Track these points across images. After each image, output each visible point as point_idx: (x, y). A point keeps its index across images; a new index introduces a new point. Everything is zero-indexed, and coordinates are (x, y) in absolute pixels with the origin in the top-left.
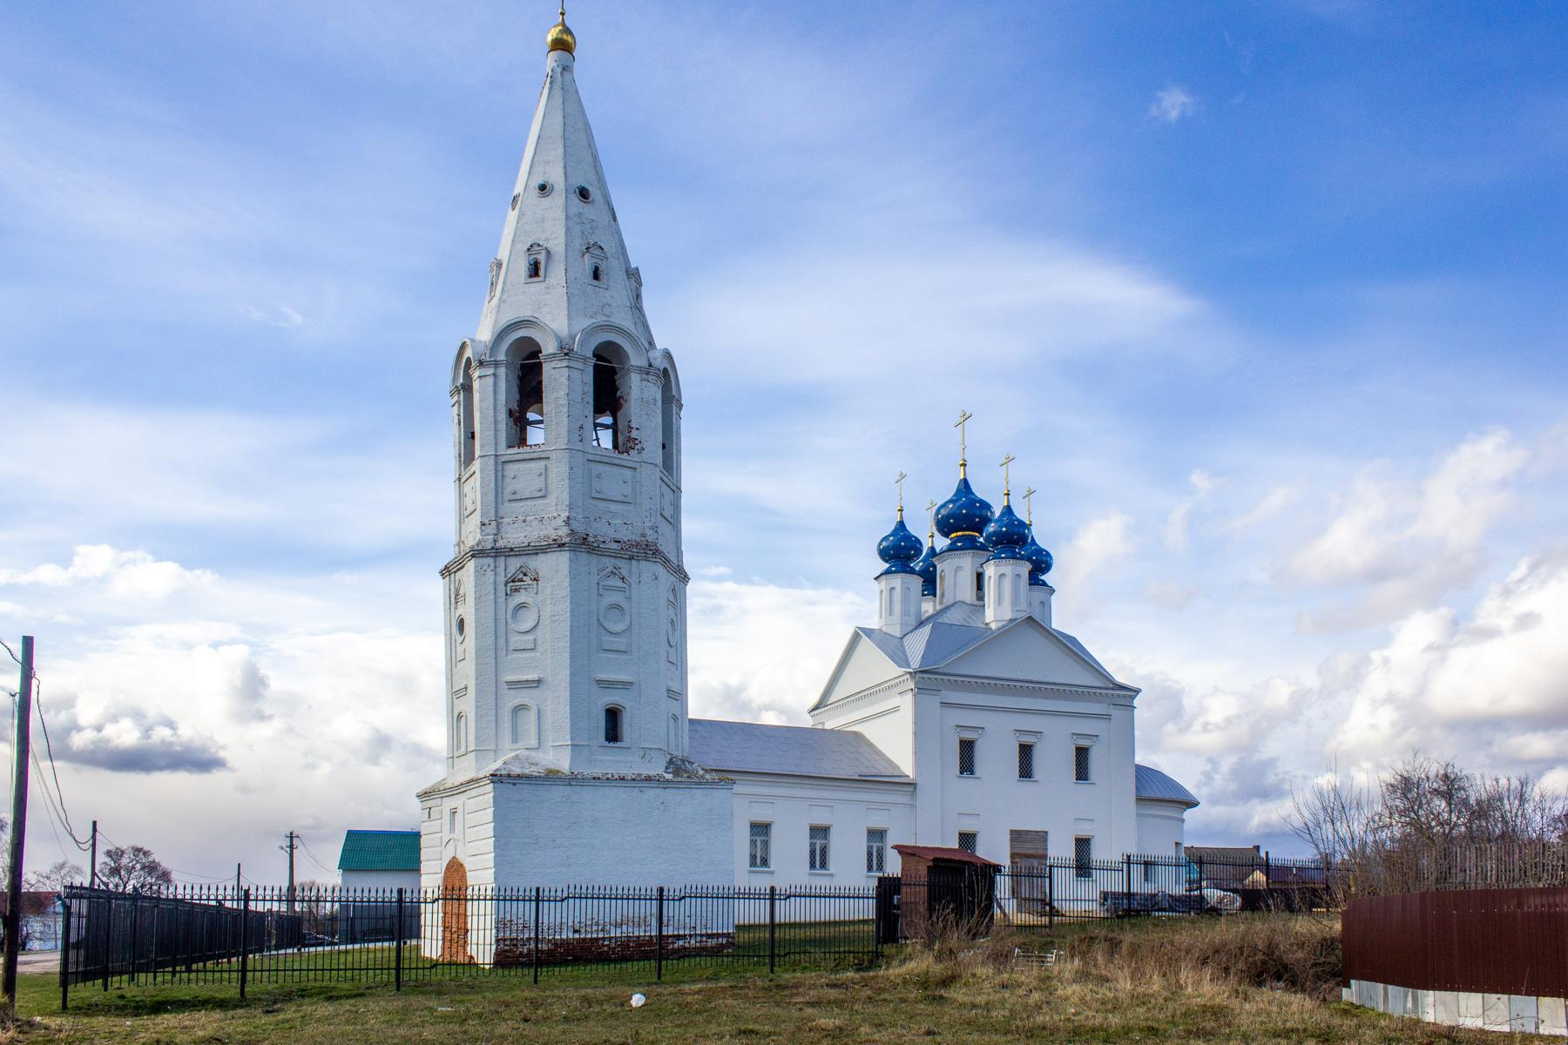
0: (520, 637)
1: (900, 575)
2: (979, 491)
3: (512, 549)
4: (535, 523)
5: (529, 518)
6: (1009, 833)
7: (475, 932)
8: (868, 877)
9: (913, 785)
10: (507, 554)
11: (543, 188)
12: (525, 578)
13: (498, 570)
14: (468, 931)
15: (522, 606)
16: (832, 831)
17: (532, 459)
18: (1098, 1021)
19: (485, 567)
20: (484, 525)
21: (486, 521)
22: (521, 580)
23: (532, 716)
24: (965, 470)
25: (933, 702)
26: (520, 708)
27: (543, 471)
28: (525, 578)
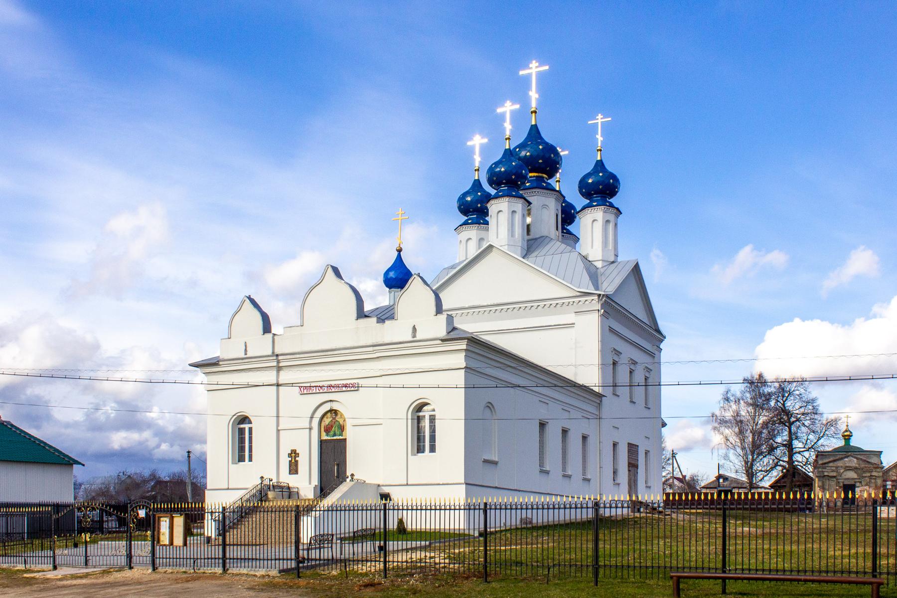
1: (507, 199)
9: (600, 396)
24: (535, 116)
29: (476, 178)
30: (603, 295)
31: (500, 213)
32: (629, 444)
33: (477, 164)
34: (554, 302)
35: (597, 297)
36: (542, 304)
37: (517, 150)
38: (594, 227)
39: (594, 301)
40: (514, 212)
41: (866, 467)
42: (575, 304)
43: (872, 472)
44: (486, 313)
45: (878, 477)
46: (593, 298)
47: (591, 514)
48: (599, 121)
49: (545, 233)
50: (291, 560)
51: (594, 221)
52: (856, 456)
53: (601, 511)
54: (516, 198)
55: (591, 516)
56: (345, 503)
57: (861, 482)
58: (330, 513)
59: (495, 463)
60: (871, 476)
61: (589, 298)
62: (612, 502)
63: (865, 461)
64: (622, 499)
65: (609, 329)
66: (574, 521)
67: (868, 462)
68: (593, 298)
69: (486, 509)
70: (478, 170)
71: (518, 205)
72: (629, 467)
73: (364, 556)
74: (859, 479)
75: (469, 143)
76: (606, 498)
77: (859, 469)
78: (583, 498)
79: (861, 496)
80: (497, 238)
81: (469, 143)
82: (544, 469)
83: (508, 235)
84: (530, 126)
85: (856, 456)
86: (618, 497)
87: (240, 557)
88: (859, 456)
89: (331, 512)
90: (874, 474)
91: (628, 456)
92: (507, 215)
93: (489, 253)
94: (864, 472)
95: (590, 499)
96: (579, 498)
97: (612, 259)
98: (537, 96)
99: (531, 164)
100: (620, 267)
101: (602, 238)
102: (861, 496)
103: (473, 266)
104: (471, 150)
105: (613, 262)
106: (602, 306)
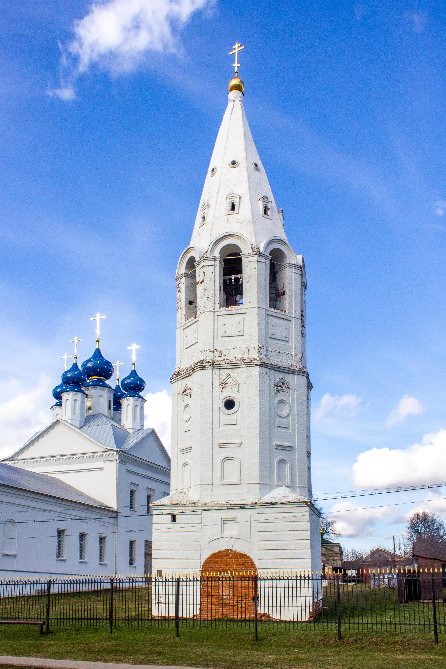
0: (280, 419)
1: (71, 393)
2: (106, 356)
3: (279, 367)
4: (285, 355)
5: (281, 351)
6: (144, 542)
7: (262, 599)
8: (100, 564)
9: (117, 512)
10: (275, 369)
11: (234, 163)
12: (282, 386)
13: (271, 377)
14: (258, 598)
15: (282, 402)
16: (66, 533)
17: (282, 318)
18: (114, 649)
19: (265, 374)
20: (260, 348)
21: (261, 346)
22: (281, 387)
23: (287, 467)
24: (98, 344)
25: (124, 468)
26: (282, 461)
27: (288, 327)
28: (282, 386)
29: (133, 369)
30: (120, 451)
31: (68, 401)
32: (146, 541)
33: (134, 361)
34: (92, 455)
35: (115, 452)
36: (85, 456)
37: (85, 363)
38: (128, 410)
39: (114, 455)
40: (75, 400)
41: (330, 553)
42: (104, 456)
43: (334, 556)
44: (67, 459)
45: (338, 560)
46: (113, 453)
47: (109, 586)
48: (66, 357)
49: (100, 412)
50: (106, 619)
51: (128, 405)
52: (325, 546)
53: (115, 585)
54: (77, 393)
55: (325, 585)
56: (36, 579)
57: (328, 563)
58: (19, 585)
59: (15, 556)
60: (334, 559)
61: (112, 453)
62: (130, 579)
63: (329, 549)
64: (139, 577)
65: (126, 471)
66: (81, 591)
67: (331, 550)
68: (113, 453)
69: (49, 583)
70: (134, 364)
71: (79, 396)
72: (145, 555)
73: (92, 616)
74: (327, 561)
75: (129, 348)
76: (120, 576)
77: (327, 554)
78: (102, 576)
79: (328, 573)
80: (65, 415)
81: (129, 348)
82: (62, 559)
83: (71, 414)
84: (95, 349)
85: (325, 546)
86: (140, 575)
87: (87, 618)
88: (326, 547)
89: (125, 583)
90: (335, 558)
91: (145, 549)
92: (71, 401)
93: (57, 425)
94: (330, 557)
95: (108, 577)
96: (106, 577)
97: (139, 428)
98: (99, 332)
99: (89, 372)
100: (143, 432)
101: (132, 415)
102: (328, 573)
103: (51, 430)
104: (130, 352)
105: (139, 430)
106: (119, 457)
